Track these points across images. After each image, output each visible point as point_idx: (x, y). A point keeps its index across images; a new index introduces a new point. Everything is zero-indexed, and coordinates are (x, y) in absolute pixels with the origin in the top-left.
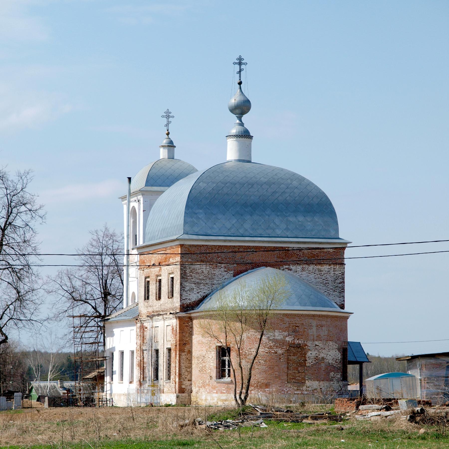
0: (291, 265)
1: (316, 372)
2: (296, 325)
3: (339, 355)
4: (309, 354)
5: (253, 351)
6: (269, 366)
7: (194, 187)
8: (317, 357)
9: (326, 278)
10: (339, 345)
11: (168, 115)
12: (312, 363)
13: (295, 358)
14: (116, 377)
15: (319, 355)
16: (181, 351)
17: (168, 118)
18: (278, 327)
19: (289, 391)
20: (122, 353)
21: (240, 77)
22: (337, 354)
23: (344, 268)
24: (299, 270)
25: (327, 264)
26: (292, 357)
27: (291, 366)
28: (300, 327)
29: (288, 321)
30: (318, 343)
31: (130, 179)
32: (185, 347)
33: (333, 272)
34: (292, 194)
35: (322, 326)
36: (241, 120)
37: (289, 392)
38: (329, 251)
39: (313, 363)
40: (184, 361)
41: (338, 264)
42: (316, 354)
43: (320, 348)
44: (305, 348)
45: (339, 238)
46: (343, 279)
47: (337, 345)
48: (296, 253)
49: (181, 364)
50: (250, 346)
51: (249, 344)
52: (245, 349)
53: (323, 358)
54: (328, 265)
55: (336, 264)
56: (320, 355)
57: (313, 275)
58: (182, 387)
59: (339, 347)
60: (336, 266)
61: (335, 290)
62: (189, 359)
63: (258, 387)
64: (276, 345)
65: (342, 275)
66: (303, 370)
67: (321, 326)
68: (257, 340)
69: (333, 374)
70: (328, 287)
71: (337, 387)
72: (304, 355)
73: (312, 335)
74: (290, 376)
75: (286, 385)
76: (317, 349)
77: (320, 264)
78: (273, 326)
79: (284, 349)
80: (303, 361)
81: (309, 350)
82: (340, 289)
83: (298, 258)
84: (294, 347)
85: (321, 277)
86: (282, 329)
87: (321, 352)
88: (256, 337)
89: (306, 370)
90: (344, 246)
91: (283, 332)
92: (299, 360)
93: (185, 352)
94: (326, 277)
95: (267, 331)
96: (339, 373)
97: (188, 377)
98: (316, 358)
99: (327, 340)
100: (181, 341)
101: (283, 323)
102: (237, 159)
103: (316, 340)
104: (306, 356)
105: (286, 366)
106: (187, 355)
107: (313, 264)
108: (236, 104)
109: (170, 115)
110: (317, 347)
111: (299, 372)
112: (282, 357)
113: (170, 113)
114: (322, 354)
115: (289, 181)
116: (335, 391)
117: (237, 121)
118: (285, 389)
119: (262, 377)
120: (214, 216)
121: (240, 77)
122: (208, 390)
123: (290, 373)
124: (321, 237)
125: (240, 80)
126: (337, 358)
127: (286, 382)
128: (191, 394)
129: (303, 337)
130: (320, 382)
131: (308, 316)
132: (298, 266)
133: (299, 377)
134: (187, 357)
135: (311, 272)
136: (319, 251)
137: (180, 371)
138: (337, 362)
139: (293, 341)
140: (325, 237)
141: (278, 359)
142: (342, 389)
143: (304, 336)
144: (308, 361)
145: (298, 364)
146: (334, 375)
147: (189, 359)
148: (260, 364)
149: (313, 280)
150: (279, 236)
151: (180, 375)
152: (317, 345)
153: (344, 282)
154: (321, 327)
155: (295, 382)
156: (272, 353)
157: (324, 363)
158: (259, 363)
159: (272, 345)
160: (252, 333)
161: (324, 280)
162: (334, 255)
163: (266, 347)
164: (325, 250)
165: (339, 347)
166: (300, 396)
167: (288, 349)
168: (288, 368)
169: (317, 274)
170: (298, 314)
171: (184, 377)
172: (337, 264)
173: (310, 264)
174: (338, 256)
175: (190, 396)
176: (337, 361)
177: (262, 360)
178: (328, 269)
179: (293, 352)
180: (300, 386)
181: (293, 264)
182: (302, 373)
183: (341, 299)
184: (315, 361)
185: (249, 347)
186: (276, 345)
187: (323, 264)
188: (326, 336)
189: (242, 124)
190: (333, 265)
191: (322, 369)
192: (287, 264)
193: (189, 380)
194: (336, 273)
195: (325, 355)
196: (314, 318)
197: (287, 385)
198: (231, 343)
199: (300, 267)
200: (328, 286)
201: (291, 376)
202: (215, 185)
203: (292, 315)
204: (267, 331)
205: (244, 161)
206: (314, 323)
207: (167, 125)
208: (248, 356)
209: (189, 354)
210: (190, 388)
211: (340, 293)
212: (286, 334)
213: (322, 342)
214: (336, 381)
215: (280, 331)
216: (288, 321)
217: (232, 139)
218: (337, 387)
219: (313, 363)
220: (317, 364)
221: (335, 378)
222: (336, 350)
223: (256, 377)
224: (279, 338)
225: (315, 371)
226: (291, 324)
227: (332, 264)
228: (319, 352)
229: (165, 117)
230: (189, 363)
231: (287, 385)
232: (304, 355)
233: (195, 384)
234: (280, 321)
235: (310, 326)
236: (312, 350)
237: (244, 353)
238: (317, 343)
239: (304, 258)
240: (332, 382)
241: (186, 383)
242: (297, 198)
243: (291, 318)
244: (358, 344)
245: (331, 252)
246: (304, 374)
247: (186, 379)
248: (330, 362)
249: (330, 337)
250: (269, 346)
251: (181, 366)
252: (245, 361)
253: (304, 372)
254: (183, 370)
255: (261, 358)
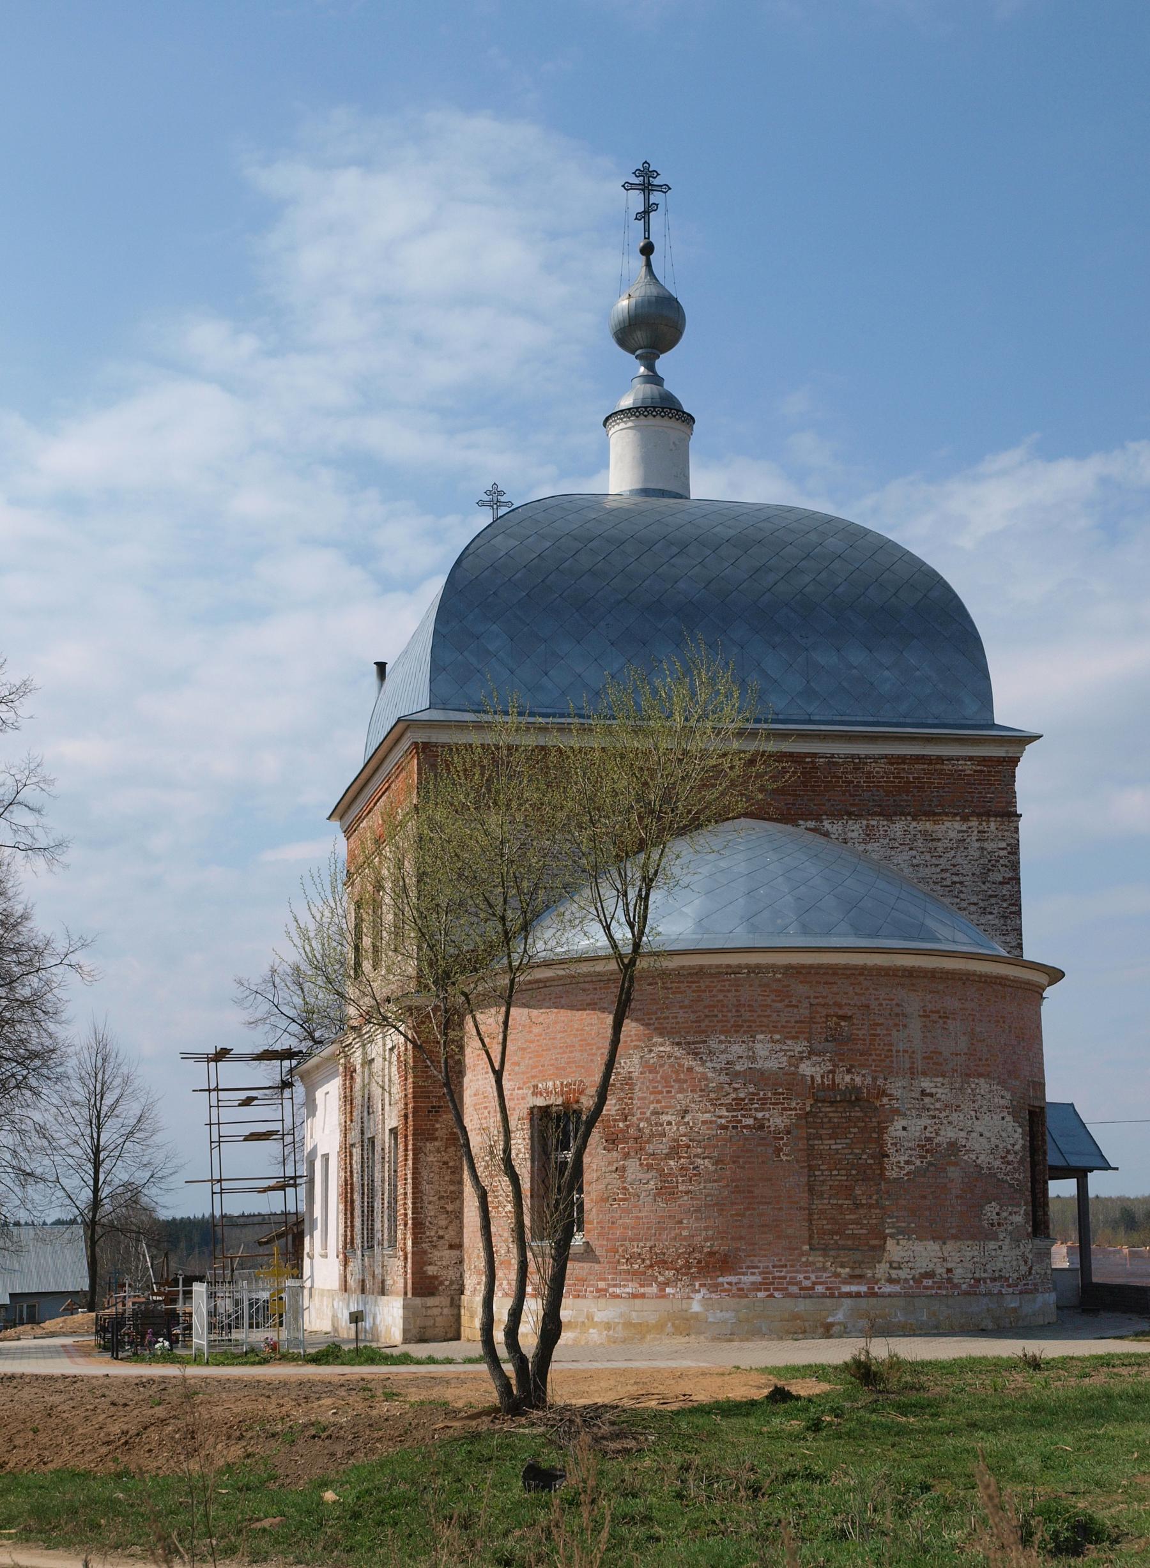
0: (824, 817)
1: (928, 1202)
2: (840, 1013)
3: (1017, 1136)
4: (895, 1129)
5: (669, 1123)
6: (733, 1181)
7: (470, 551)
8: (928, 1139)
9: (954, 866)
10: (1013, 1094)
11: (495, 499)
12: (908, 1168)
13: (840, 1146)
14: (317, 1234)
15: (937, 1134)
16: (419, 1134)
17: (495, 506)
18: (765, 1020)
19: (821, 1283)
20: (326, 1157)
21: (647, 229)
22: (1010, 1129)
23: (1017, 828)
24: (855, 835)
25: (956, 815)
26: (826, 1142)
27: (821, 1178)
28: (855, 1021)
29: (808, 997)
30: (932, 1085)
31: (381, 667)
32: (437, 1121)
33: (977, 845)
34: (824, 575)
35: (948, 1018)
36: (650, 367)
37: (817, 1287)
38: (960, 767)
39: (913, 1167)
40: (432, 1175)
41: (996, 816)
42: (926, 1128)
43: (938, 1105)
44: (878, 1104)
45: (994, 726)
46: (1015, 866)
47: (1009, 1097)
48: (841, 777)
49: (420, 1183)
50: (658, 1102)
51: (651, 1093)
52: (639, 1116)
53: (953, 1145)
54: (958, 818)
55: (988, 814)
56: (942, 1133)
57: (907, 855)
58: (425, 1272)
59: (1015, 1103)
60: (988, 822)
61: (985, 909)
62: (451, 1164)
63: (690, 1268)
64: (762, 1093)
65: (1009, 853)
66: (874, 1197)
67: (942, 1014)
68: (682, 1076)
69: (997, 1210)
70: (962, 896)
71: (1015, 1263)
72: (875, 1135)
73: (907, 1052)
74: (820, 1222)
75: (804, 1259)
76: (928, 1110)
77: (930, 814)
78: (747, 1015)
79: (794, 1113)
80: (872, 1157)
81: (897, 1112)
82: (1005, 905)
83: (850, 795)
84: (836, 1102)
85: (934, 861)
86: (783, 1027)
87: (945, 1122)
88: (679, 1065)
89: (886, 1196)
90: (1010, 751)
91: (789, 1042)
92: (856, 1154)
93: (436, 1139)
94: (954, 861)
95: (723, 1038)
96: (1018, 1205)
97: (450, 1235)
98: (926, 1147)
99: (968, 1072)
100: (420, 1097)
101: (788, 1006)
102: (638, 486)
103: (924, 1074)
104: (885, 1137)
105: (804, 1179)
106: (445, 1151)
107: (902, 814)
108: (632, 312)
109: (502, 499)
110: (927, 1100)
111: (858, 1206)
112: (784, 1145)
113: (502, 493)
114: (949, 1129)
115: (813, 537)
116: (1007, 1279)
117: (638, 370)
118: (800, 1277)
119: (706, 1228)
120: (543, 646)
121: (647, 229)
122: (505, 1282)
123: (820, 1207)
124: (929, 721)
125: (648, 238)
126: (1010, 1147)
127: (806, 1247)
128: (460, 1299)
129: (870, 1058)
130: (944, 1243)
131: (887, 975)
132: (850, 822)
133: (857, 1224)
134: (446, 1158)
135: (897, 845)
136: (924, 770)
137: (417, 1213)
138: (1009, 1163)
139: (831, 1076)
140: (946, 721)
141: (770, 1150)
142: (1031, 1268)
143: (874, 1057)
144: (893, 1160)
145: (854, 1172)
146: (998, 1214)
147: (451, 1164)
148: (695, 1175)
149: (908, 871)
150: (781, 717)
151: (419, 1227)
152: (928, 1091)
153: (1017, 880)
154: (941, 1021)
155: (844, 1248)
156: (745, 1127)
157: (956, 1164)
158: (694, 1169)
159: (742, 1095)
160: (662, 1049)
161: (946, 870)
162: (978, 784)
163: (721, 1105)
164: (947, 767)
165: (1015, 1103)
166: (863, 1303)
167: (808, 1109)
168: (811, 1190)
169: (921, 850)
170: (846, 967)
171: (433, 1234)
172: (989, 816)
173: (895, 814)
174: (993, 787)
175: (459, 1307)
176: (1010, 1158)
177: (704, 1158)
178: (959, 832)
179: (830, 1122)
180: (863, 1262)
181: (833, 815)
182: (871, 1206)
183: (1008, 939)
184: (921, 1157)
185: (652, 1107)
186: (762, 1093)
187: (939, 814)
188: (964, 1058)
189: (654, 378)
190: (975, 819)
191: (954, 1191)
192: (811, 814)
193: (451, 1247)
194: (989, 846)
195: (963, 1134)
196: (913, 985)
197: (810, 1259)
198: (582, 1092)
199: (858, 826)
200: (961, 892)
201: (825, 1222)
202: (548, 544)
203: (822, 971)
204: (723, 1038)
205: (662, 493)
206: (913, 1002)
207: (645, 215)
208: (648, 1142)
209: (453, 1148)
210: (458, 1275)
211: (1006, 917)
212: (800, 1049)
213: (946, 1081)
214: (1007, 1241)
215: (777, 1037)
216: (808, 997)
217: (622, 425)
218: (1015, 1263)
219: (913, 1167)
220: (931, 1168)
221: (1002, 1228)
222: (1005, 1114)
223: (684, 1228)
224: (772, 1065)
225: (924, 1197)
226: (819, 1009)
227: (974, 813)
228: (937, 1121)
229: (488, 503)
230: (452, 1182)
231: (810, 1259)
232: (875, 1135)
233: (469, 1258)
234: (773, 997)
235: (897, 1015)
236: (908, 1113)
237: (632, 1131)
238: (926, 1084)
239: (873, 795)
240: (992, 1245)
241: (441, 1257)
242: (841, 589)
243: (818, 983)
244: (1069, 1109)
245: (968, 772)
246: (877, 1211)
247: (441, 1242)
248: (983, 1159)
249: (980, 1060)
250: (733, 1100)
251: (421, 1192)
252: (638, 1163)
253: (877, 1205)
254: (430, 1207)
255: (699, 1150)
